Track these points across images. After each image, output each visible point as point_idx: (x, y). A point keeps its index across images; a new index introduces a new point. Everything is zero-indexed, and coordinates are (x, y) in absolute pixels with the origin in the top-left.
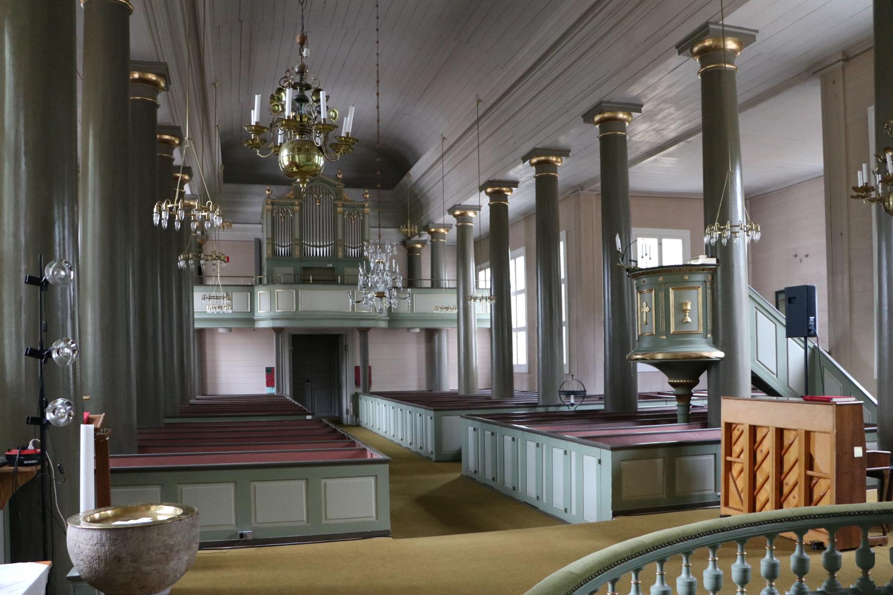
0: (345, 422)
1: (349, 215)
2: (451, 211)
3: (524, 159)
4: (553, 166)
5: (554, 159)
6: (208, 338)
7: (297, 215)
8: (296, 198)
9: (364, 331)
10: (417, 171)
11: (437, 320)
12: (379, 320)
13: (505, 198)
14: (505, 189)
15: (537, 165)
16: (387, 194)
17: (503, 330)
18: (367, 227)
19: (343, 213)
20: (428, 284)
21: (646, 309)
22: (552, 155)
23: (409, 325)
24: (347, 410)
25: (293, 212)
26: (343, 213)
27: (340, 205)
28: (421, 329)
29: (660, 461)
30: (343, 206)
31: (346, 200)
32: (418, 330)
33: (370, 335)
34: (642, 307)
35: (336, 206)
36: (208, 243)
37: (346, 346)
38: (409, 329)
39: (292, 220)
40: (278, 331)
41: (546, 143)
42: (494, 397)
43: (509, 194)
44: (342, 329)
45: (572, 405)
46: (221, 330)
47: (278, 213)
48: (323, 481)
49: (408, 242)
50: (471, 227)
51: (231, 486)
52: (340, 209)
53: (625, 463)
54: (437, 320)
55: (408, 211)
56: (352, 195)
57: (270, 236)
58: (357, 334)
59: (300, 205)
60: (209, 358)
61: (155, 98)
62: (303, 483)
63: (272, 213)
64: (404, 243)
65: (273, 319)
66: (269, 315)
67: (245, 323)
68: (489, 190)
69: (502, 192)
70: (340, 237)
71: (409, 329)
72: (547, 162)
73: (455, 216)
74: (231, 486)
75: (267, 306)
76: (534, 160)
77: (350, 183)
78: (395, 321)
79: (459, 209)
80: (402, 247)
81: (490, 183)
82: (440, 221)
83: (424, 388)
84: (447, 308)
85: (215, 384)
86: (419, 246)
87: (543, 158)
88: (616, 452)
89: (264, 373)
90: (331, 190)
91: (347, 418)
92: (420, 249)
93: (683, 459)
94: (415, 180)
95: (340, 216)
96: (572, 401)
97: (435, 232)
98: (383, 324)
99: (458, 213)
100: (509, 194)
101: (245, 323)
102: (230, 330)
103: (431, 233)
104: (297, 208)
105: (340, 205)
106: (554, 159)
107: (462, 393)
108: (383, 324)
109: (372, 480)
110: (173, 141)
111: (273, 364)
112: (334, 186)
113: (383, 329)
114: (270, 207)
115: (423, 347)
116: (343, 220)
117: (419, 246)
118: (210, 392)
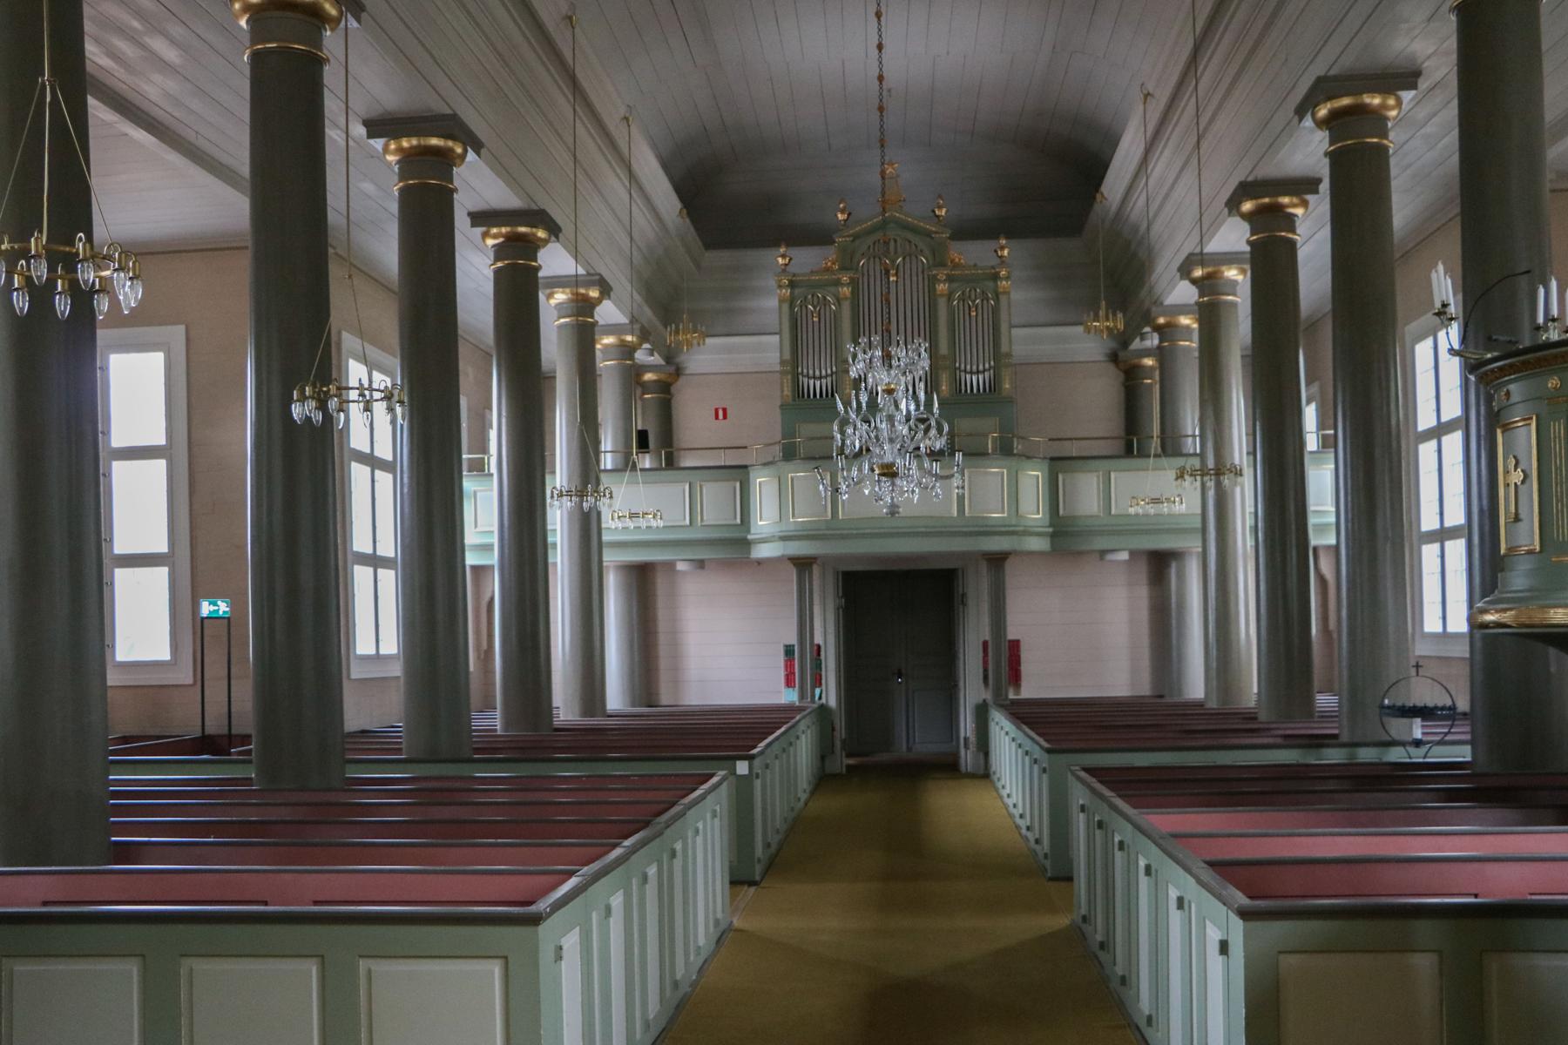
0: (963, 769)
1: (962, 299)
2: (1185, 271)
3: (1301, 112)
4: (1376, 121)
5: (1376, 101)
6: (661, 583)
8: (843, 268)
9: (997, 561)
10: (1114, 186)
11: (1168, 531)
12: (1027, 533)
13: (1290, 222)
14: (1285, 200)
15: (1332, 123)
17: (1284, 553)
18: (1004, 327)
19: (950, 297)
20: (1155, 444)
21: (1517, 477)
22: (1285, 194)
23: (1100, 543)
24: (966, 739)
25: (839, 301)
26: (950, 297)
28: (1133, 553)
29: (1424, 964)
30: (950, 279)
31: (956, 266)
32: (1124, 556)
33: (1009, 567)
34: (1507, 472)
35: (933, 280)
36: (682, 381)
37: (963, 595)
38: (1103, 553)
39: (837, 316)
40: (803, 564)
41: (1347, 63)
42: (1263, 716)
43: (1299, 211)
44: (951, 555)
45: (1418, 743)
46: (681, 566)
47: (804, 305)
48: (363, 964)
49: (1122, 354)
50: (1234, 305)
51: (133, 968)
52: (942, 287)
53: (1293, 960)
54: (1168, 531)
55: (1112, 277)
56: (972, 254)
57: (787, 356)
58: (984, 567)
59: (854, 283)
60: (662, 625)
61: (317, 42)
62: (313, 969)
63: (792, 307)
64: (1114, 358)
65: (784, 538)
66: (775, 530)
67: (730, 549)
68: (1247, 206)
69: (1279, 208)
70: (944, 348)
71: (1103, 553)
72: (1360, 110)
73: (1194, 282)
74: (133, 968)
75: (775, 511)
76: (1323, 112)
77: (966, 231)
78: (1068, 539)
79: (1203, 264)
80: (1112, 367)
81: (1246, 189)
82: (1171, 300)
83: (1145, 689)
84: (1156, 501)
85: (677, 682)
87: (1346, 101)
88: (1258, 925)
89: (781, 659)
90: (921, 245)
91: (968, 758)
93: (1518, 960)
94: (1114, 208)
95: (942, 303)
96: (1418, 733)
97: (1168, 325)
98: (1037, 544)
100: (1299, 211)
101: (730, 549)
103: (1158, 329)
106: (1376, 101)
107: (1213, 704)
108: (1037, 544)
109: (496, 968)
110: (451, 150)
111: (793, 639)
112: (928, 234)
113: (1041, 553)
114: (787, 292)
115: (1143, 592)
118: (665, 698)
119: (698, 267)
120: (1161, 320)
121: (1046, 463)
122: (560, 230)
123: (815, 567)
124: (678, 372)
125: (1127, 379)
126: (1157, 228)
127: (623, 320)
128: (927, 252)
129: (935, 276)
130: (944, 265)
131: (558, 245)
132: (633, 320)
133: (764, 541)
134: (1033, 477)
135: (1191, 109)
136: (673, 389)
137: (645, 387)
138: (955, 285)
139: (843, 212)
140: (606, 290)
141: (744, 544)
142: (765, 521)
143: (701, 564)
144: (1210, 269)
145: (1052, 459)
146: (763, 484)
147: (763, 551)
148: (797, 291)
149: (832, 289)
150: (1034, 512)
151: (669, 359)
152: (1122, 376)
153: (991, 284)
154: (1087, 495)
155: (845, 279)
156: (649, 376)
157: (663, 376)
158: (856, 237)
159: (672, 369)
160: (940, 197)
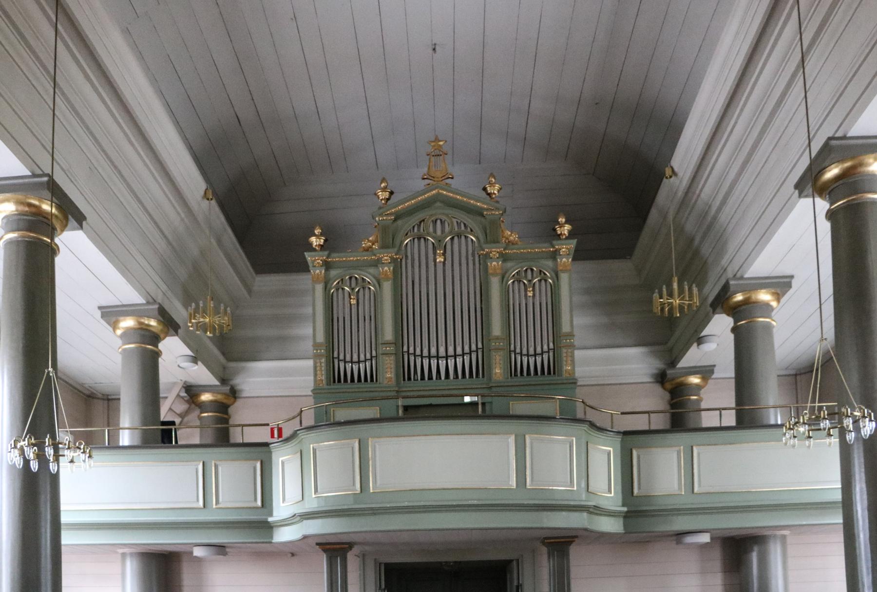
7: (387, 286)
8: (384, 246)
9: (560, 544)
12: (596, 511)
16: (621, 270)
27: (494, 254)
30: (505, 258)
33: (575, 552)
36: (239, 403)
39: (376, 299)
40: (335, 550)
49: (670, 372)
52: (494, 264)
59: (397, 264)
63: (326, 288)
64: (661, 378)
78: (643, 524)
80: (658, 389)
86: (695, 380)
92: (698, 387)
95: (495, 282)
97: (746, 302)
99: (832, 172)
102: (221, 549)
104: (388, 269)
105: (494, 254)
108: (610, 525)
112: (479, 213)
116: (505, 293)
117: (695, 380)
119: (250, 291)
120: (739, 297)
121: (618, 439)
122: (85, 218)
123: (350, 556)
124: (234, 393)
125: (673, 406)
126: (723, 217)
127: (140, 300)
128: (477, 229)
129: (487, 256)
130: (496, 241)
131: (80, 233)
132: (151, 301)
133: (285, 523)
134: (604, 454)
135: (792, 26)
136: (231, 410)
137: (202, 407)
138: (509, 264)
139: (384, 190)
140: (71, 214)
141: (265, 527)
142: (287, 499)
143: (221, 549)
144: (848, 164)
145: (626, 433)
146: (285, 463)
147: (285, 535)
148: (333, 273)
149: (372, 270)
150: (606, 489)
151: (224, 381)
152: (667, 396)
153: (550, 263)
154: (666, 471)
155: (386, 258)
156: (206, 397)
157: (219, 397)
158: (398, 217)
159: (227, 389)
160: (492, 175)
